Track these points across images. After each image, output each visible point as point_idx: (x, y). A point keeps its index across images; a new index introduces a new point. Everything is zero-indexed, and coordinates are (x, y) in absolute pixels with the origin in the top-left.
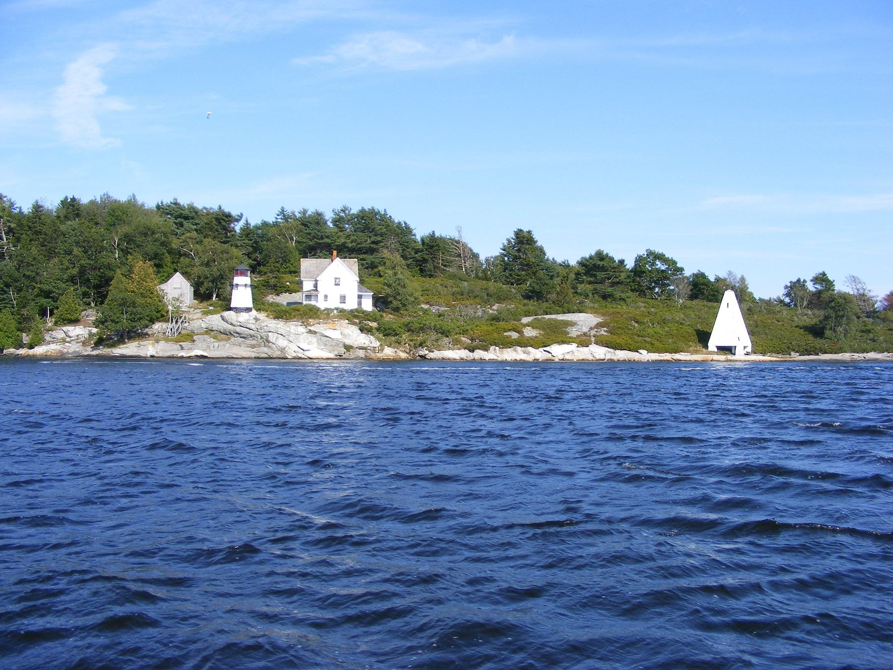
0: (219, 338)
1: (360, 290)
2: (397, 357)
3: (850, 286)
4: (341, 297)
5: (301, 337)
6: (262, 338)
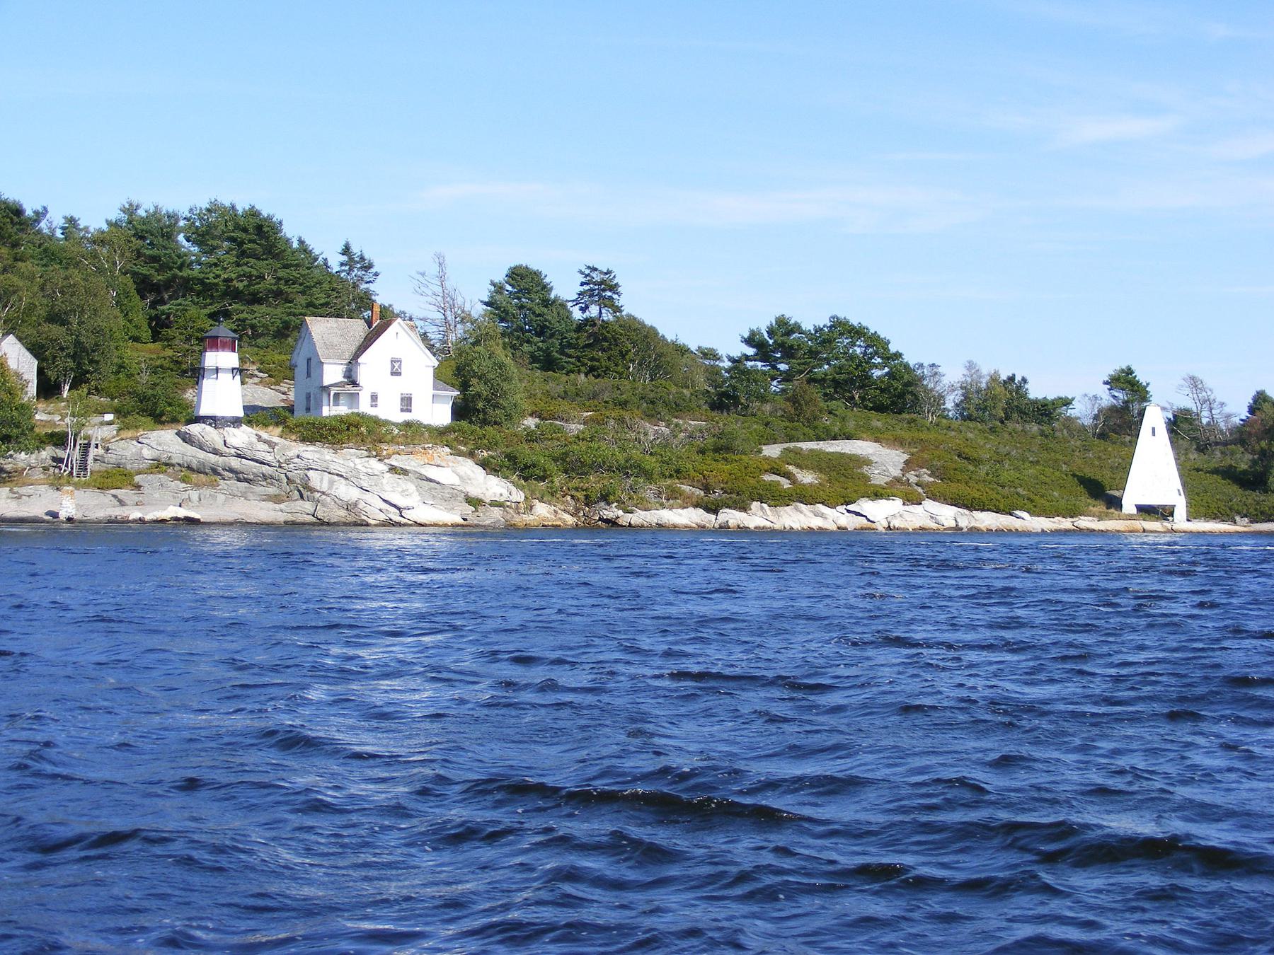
1: (435, 388)
3: (1190, 395)
4: (402, 399)
5: (385, 481)
6: (289, 481)
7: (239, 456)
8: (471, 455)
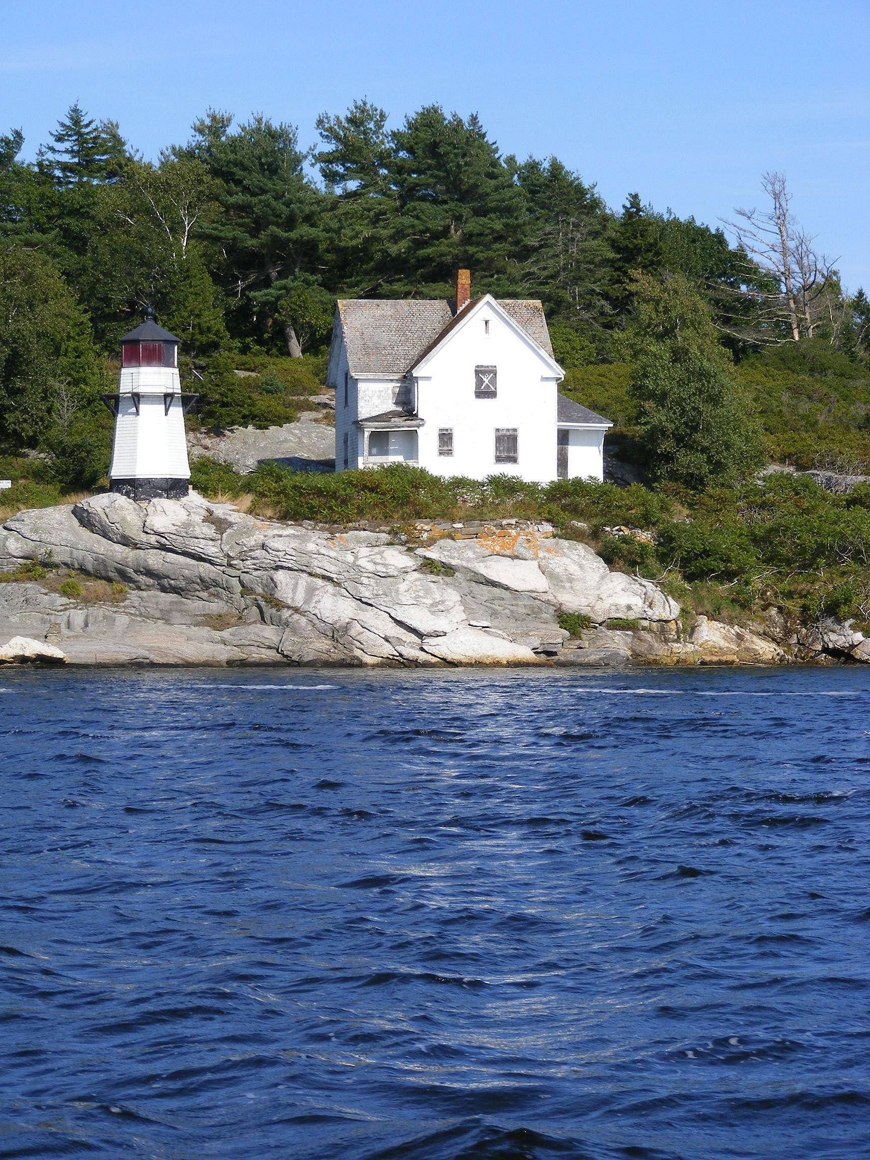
0: (83, 592)
1: (563, 413)
2: (746, 656)
5: (403, 587)
6: (246, 590)
7: (163, 548)
8: (595, 535)
